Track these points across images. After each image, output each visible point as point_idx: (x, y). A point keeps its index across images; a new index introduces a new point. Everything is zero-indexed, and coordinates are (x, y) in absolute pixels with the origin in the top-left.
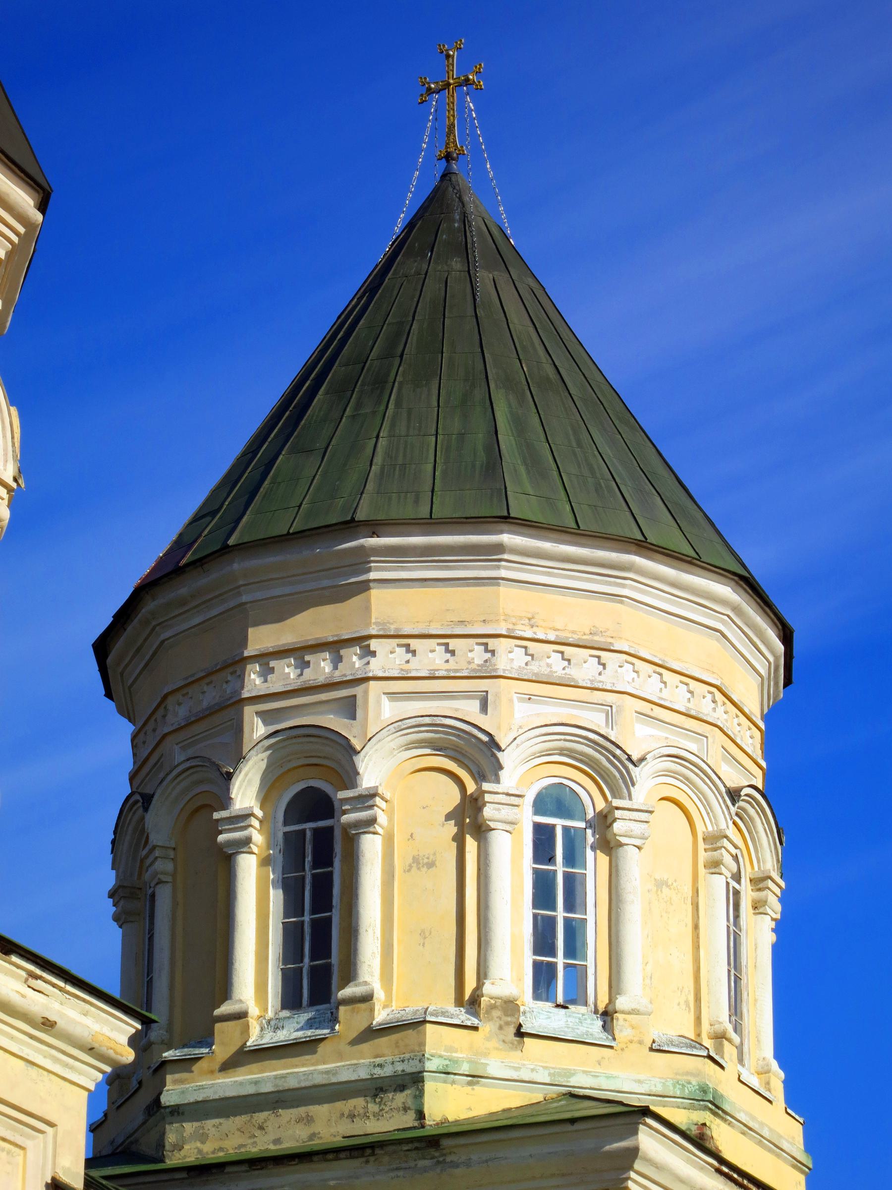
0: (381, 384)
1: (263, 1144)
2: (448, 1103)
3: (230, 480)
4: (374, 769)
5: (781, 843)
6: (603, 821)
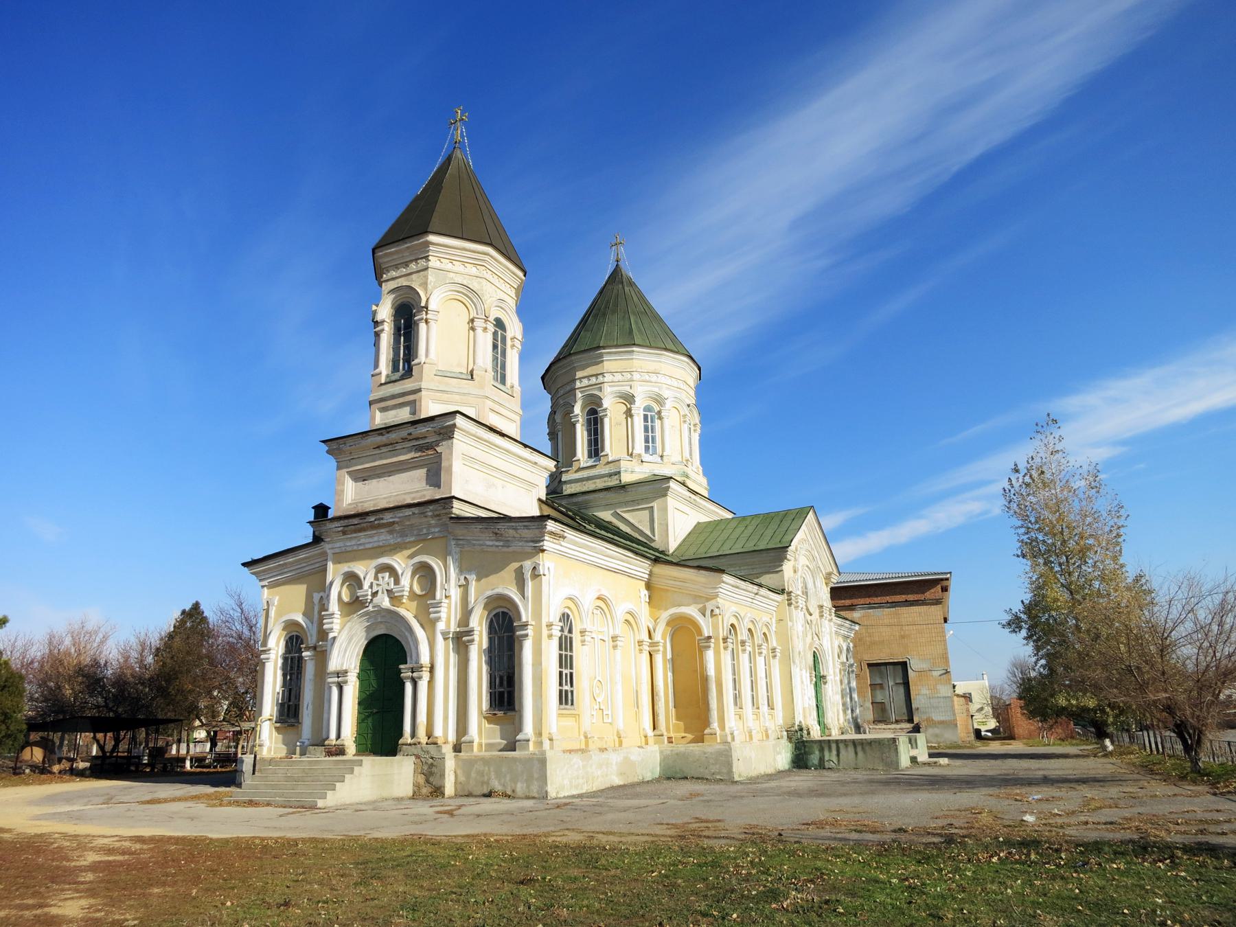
0: (604, 315)
1: (585, 489)
2: (626, 478)
3: (570, 338)
4: (606, 403)
5: (406, 264)
6: (659, 412)
